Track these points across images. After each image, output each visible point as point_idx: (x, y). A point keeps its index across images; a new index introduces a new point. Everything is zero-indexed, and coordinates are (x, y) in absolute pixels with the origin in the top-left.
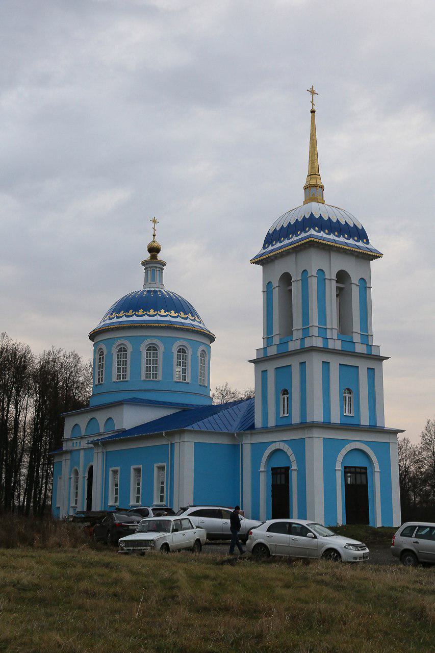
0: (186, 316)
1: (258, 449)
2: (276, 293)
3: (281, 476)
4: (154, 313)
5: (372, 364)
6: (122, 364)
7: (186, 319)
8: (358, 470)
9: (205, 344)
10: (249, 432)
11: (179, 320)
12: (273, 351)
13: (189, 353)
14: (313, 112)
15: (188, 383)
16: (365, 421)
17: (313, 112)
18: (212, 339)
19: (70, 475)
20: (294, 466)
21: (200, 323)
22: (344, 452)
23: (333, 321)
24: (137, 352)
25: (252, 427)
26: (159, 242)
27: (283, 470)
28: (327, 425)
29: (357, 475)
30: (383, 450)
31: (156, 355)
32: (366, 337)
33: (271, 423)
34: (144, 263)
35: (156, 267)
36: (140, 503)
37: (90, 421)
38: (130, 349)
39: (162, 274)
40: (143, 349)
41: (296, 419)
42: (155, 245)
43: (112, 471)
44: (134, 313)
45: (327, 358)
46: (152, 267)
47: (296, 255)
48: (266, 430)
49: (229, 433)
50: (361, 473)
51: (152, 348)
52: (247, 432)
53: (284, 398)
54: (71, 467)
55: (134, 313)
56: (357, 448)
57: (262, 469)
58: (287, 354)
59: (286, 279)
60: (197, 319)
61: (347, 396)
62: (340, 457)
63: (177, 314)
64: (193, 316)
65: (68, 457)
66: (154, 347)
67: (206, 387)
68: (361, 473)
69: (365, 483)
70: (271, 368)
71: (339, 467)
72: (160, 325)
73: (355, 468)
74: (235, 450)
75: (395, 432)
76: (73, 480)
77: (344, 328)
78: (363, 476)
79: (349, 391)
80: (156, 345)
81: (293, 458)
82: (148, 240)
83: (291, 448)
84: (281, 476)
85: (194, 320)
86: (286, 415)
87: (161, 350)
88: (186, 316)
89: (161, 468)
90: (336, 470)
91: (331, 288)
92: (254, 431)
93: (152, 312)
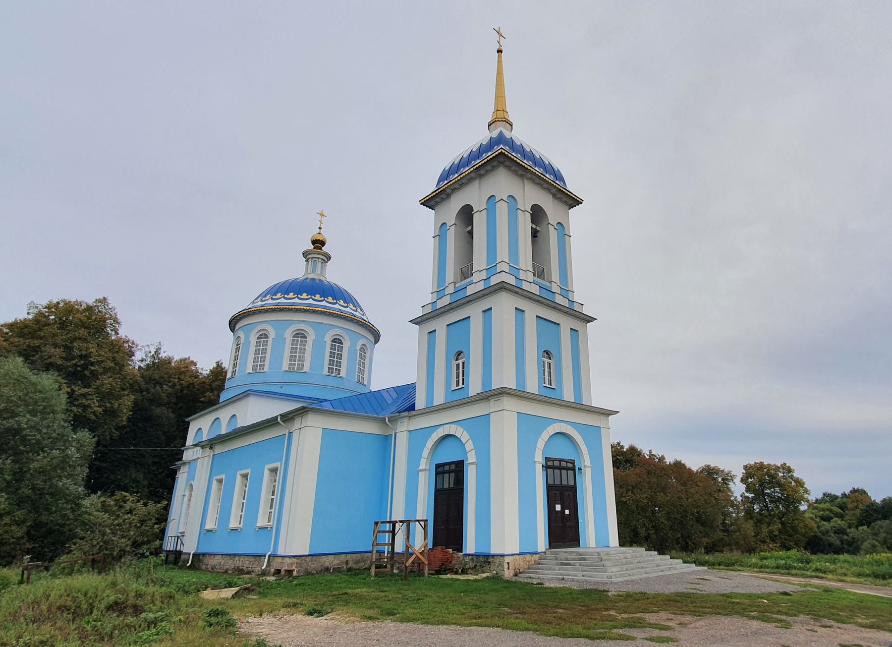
0: (346, 305)
1: (419, 438)
2: (451, 235)
3: (449, 475)
4: (307, 297)
5: (576, 325)
6: (260, 354)
7: (347, 307)
8: (564, 464)
9: (367, 338)
10: (406, 413)
11: (336, 306)
12: (446, 301)
13: (346, 345)
14: (500, 51)
15: (343, 378)
16: (568, 395)
17: (500, 51)
18: (377, 336)
19: (185, 492)
20: (471, 458)
21: (363, 315)
22: (545, 435)
23: (526, 261)
24: (280, 338)
25: (412, 407)
26: (326, 235)
27: (453, 467)
28: (519, 394)
29: (562, 471)
30: (593, 434)
31: (304, 343)
32: (566, 292)
33: (439, 399)
34: (306, 254)
35: (318, 258)
36: (241, 525)
37: (213, 422)
38: (272, 334)
39: (325, 268)
40: (288, 335)
41: (475, 387)
42: (320, 238)
43: (216, 480)
44: (283, 295)
45: (523, 304)
46: (314, 258)
47: (479, 181)
48: (431, 410)
49: (378, 418)
50: (567, 469)
51: (300, 335)
52: (403, 414)
53: (458, 365)
54: (188, 480)
55: (283, 295)
56: (556, 432)
57: (422, 466)
58: (464, 301)
59: (467, 214)
60: (359, 310)
61: (547, 360)
62: (541, 444)
63: (335, 301)
64: (354, 306)
65: (187, 466)
66: (302, 334)
67: (365, 385)
68: (567, 469)
69: (573, 484)
70: (440, 325)
71: (539, 459)
72: (311, 308)
73: (560, 460)
74: (386, 441)
75: (607, 413)
76: (186, 498)
77: (540, 272)
78: (571, 473)
79: (547, 353)
80: (305, 331)
81: (469, 446)
82: (313, 233)
83: (467, 431)
84: (449, 475)
85: (356, 311)
86: (461, 386)
87: (311, 337)
88: (346, 305)
89: (274, 471)
90: (535, 462)
91: (525, 224)
92: (413, 413)
93: (304, 296)
